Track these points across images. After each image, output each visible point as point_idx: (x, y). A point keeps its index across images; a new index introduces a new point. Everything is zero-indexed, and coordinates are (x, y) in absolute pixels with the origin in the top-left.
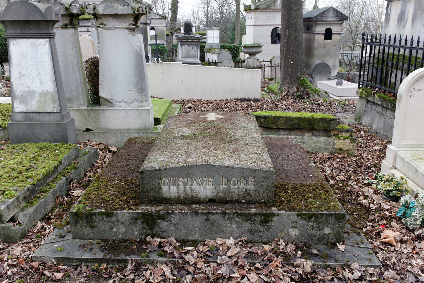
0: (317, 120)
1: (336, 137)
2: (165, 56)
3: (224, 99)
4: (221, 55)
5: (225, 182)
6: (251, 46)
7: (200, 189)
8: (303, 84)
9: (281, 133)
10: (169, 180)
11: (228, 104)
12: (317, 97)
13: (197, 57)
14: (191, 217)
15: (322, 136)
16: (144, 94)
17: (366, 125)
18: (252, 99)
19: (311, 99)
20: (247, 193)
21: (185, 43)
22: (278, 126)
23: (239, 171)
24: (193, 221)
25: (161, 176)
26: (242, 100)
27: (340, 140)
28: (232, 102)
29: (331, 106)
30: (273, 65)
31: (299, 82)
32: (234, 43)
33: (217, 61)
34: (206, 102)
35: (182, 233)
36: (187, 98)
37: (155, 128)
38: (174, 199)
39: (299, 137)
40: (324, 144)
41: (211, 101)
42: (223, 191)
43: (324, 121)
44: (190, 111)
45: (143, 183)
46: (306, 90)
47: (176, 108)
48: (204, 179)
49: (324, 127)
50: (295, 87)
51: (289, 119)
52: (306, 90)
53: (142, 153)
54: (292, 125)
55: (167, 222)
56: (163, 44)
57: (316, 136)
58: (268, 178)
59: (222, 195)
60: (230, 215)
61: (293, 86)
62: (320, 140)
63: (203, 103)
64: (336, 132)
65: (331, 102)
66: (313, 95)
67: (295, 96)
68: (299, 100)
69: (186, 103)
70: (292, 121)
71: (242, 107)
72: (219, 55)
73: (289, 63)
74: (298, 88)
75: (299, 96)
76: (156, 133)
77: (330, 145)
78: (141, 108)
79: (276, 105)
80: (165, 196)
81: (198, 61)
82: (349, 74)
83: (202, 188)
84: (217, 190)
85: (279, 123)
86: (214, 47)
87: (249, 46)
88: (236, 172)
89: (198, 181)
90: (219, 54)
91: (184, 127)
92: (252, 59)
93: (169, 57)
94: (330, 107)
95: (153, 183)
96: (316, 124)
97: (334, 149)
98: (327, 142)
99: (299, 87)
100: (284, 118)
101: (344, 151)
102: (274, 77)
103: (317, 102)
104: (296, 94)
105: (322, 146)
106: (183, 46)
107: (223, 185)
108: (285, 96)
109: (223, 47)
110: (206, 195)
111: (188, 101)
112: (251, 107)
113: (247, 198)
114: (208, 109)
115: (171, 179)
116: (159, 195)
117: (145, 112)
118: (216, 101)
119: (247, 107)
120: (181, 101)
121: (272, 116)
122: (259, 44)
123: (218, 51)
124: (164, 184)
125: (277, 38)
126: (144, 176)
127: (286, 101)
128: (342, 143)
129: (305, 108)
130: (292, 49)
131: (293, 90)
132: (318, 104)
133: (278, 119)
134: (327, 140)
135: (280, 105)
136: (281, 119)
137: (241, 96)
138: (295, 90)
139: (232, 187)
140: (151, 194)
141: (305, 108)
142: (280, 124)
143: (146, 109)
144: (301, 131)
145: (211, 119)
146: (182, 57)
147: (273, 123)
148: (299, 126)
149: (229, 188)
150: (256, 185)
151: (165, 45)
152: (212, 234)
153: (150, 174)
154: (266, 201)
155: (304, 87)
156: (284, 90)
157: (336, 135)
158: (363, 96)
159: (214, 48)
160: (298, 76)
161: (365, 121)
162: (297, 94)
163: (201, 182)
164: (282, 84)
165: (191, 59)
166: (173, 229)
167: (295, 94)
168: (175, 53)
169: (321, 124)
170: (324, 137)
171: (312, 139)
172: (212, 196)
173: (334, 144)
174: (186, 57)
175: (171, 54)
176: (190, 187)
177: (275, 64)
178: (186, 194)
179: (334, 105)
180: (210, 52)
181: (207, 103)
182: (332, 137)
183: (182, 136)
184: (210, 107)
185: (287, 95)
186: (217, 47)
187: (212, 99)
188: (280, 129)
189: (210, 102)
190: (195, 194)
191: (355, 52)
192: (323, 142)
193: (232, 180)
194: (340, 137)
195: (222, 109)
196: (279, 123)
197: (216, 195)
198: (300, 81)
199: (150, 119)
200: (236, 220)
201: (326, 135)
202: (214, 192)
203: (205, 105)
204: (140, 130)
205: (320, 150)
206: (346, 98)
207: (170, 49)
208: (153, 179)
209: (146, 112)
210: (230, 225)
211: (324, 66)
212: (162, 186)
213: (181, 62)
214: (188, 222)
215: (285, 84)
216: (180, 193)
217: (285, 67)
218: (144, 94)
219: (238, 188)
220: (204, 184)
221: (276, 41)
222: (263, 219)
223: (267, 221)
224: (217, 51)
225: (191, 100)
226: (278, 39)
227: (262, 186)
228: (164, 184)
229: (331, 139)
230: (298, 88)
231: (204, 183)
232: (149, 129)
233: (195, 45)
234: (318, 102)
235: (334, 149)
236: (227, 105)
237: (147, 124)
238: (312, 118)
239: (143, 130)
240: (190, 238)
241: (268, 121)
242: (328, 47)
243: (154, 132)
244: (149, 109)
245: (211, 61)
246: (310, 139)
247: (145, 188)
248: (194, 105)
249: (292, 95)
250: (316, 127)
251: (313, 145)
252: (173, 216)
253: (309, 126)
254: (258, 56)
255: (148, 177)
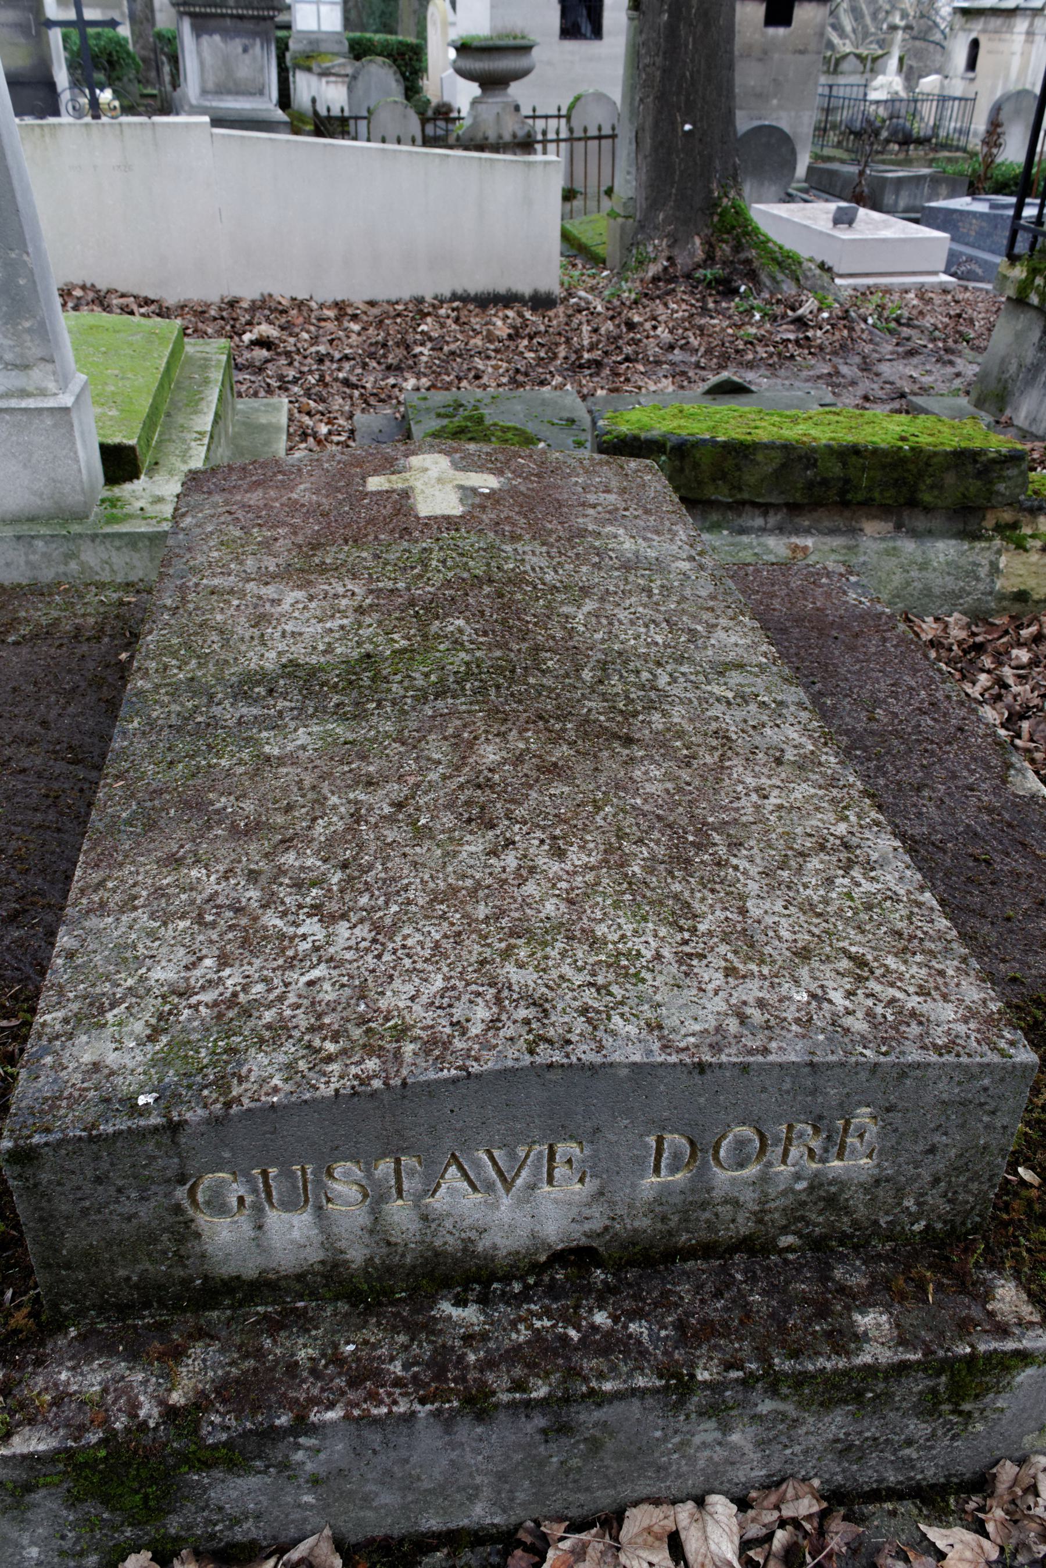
0: (935, 460)
1: (1007, 539)
2: (130, 80)
3: (406, 295)
4: (360, 84)
5: (676, 1156)
6: (490, 43)
7: (495, 1206)
8: (733, 228)
9: (750, 523)
10: (250, 1180)
11: (429, 320)
12: (789, 289)
13: (266, 91)
14: (438, 1430)
15: (944, 535)
16: (27, 324)
17: (1034, 429)
18: (523, 296)
19: (766, 295)
20: (821, 1199)
21: (212, 23)
22: (740, 490)
23: (787, 1086)
24: (453, 1445)
25: (182, 1165)
26: (487, 301)
27: (1025, 555)
28: (442, 312)
29: (851, 329)
30: (578, 133)
31: (716, 219)
32: (392, 31)
33: (346, 114)
34: (331, 314)
35: (376, 1509)
36: (248, 293)
37: (113, 502)
38: (300, 1277)
39: (837, 542)
40: (949, 574)
41: (351, 305)
42: (658, 1201)
43: (970, 468)
44: (267, 361)
45: (41, 1219)
46: (743, 256)
47: (205, 365)
48: (522, 1152)
49: (964, 495)
50: (697, 241)
51: (800, 458)
52: (743, 256)
53: (44, 723)
54: (810, 485)
55: (265, 1472)
56: (113, 24)
57: (914, 534)
58: (981, 1105)
59: (644, 1223)
60: (721, 1393)
61: (689, 239)
62: (932, 556)
63: (320, 320)
64: (1007, 516)
65: (847, 311)
66: (773, 279)
67: (699, 281)
68: (718, 298)
69: (243, 320)
70: (815, 465)
71: (490, 338)
72: (352, 81)
73: (674, 130)
74: (711, 245)
75: (718, 281)
76: (120, 536)
77: (978, 579)
78: (24, 404)
79: (631, 326)
80: (227, 1270)
81: (268, 105)
82: (862, 173)
83: (506, 1201)
84: (612, 1204)
85: (746, 477)
86: (323, 47)
87: (483, 44)
88: (764, 1090)
89: (477, 1164)
90: (354, 77)
91: (284, 575)
92: (495, 102)
93: (145, 87)
94: (845, 333)
95: (127, 1208)
96: (929, 481)
97: (991, 593)
98: (963, 561)
99: (713, 240)
100: (773, 454)
101: (1038, 602)
102: (579, 186)
103: (793, 310)
104: (702, 271)
105: (941, 582)
106: (205, 39)
107: (657, 1170)
108: (659, 280)
109: (359, 51)
110: (533, 1236)
111: (254, 308)
112: (531, 338)
113: (818, 1225)
114: (348, 351)
115: (265, 1174)
116: (179, 1272)
117: (49, 422)
118: (372, 304)
119: (510, 335)
120: (221, 309)
121: (713, 442)
122: (523, 38)
123: (345, 65)
124: (216, 1205)
125: (585, 12)
126: (45, 1177)
127: (666, 305)
128: (1034, 569)
129: (751, 343)
130: (692, 61)
131: (692, 255)
132: (801, 323)
133: (746, 457)
134: (963, 553)
135: (648, 325)
136: (760, 457)
137: (478, 283)
138: (700, 255)
139: (722, 1177)
140: (122, 1273)
141: (751, 343)
142: (752, 481)
143: (51, 410)
144: (847, 514)
145: (438, 512)
146: (204, 92)
147: (720, 475)
148: (842, 493)
149: (701, 1181)
150: (884, 1152)
151: (124, 31)
152: (588, 1489)
153: (97, 1158)
154: (939, 1226)
155: (737, 239)
156: (652, 255)
157: (1008, 530)
158: (1034, 299)
159: (326, 53)
160: (711, 192)
161: (1028, 412)
162: (709, 273)
163: (500, 1173)
164: (641, 227)
165: (241, 98)
166: (308, 1499)
167: (699, 274)
168: (166, 69)
169: (950, 478)
170: (953, 542)
171: (894, 552)
172: (576, 1235)
173: (995, 570)
174: (221, 90)
175: (153, 74)
176: (417, 1206)
177: (585, 130)
178: (389, 1244)
179: (863, 326)
180: (309, 70)
181: (337, 319)
182: (990, 539)
183: (291, 668)
184: (354, 337)
185: (666, 277)
186: (336, 48)
187: (357, 296)
188: (743, 503)
189: (350, 311)
190: (450, 1239)
191: (842, 80)
192: (948, 564)
193: (730, 1137)
194: (1025, 537)
195: (408, 348)
196: (750, 477)
197: (606, 1228)
198: (721, 215)
199: (77, 460)
200: (759, 1408)
201: (961, 527)
202: (587, 1212)
203: (330, 326)
204: (32, 519)
205: (927, 600)
206: (870, 281)
207: (143, 53)
208: (120, 1191)
209: (55, 426)
210: (718, 1435)
211: (773, 141)
212: (203, 1220)
213: (206, 119)
214: (414, 1460)
215: (656, 228)
216: (342, 1244)
217: (655, 149)
218: (27, 324)
219: (764, 1179)
220: (519, 1182)
221: (579, 28)
222: (942, 1388)
223: (957, 1393)
224: (340, 65)
225: (264, 301)
226: (589, 16)
227: (932, 1150)
228: (216, 1205)
229: (982, 549)
230: (711, 245)
231: (524, 1173)
232: (80, 517)
233: (254, 34)
234: (800, 312)
235: (991, 593)
236: (423, 327)
237: (67, 490)
238: (912, 449)
239: (48, 519)
240: (432, 1523)
241: (696, 465)
242: (776, 56)
243: (108, 530)
244: (66, 410)
245: (323, 112)
246: (887, 552)
247: (69, 1244)
248: (282, 328)
249: (688, 276)
250: (927, 497)
251: (897, 579)
252: (302, 1440)
253: (892, 492)
254: (515, 89)
255: (76, 1180)
